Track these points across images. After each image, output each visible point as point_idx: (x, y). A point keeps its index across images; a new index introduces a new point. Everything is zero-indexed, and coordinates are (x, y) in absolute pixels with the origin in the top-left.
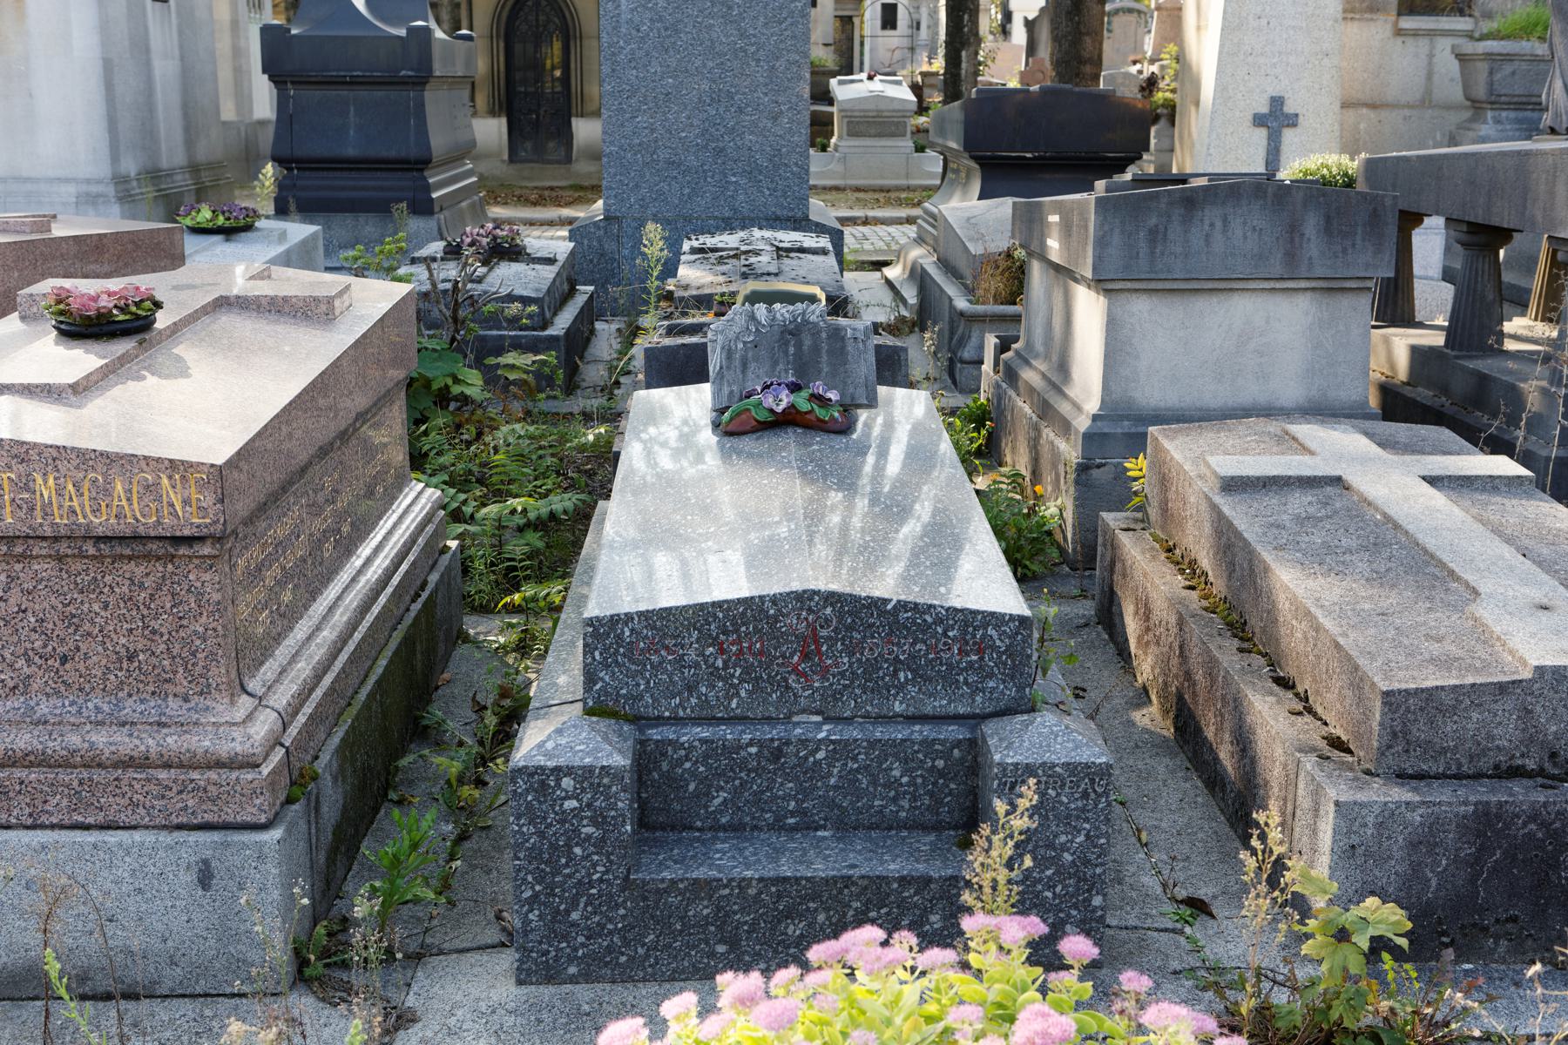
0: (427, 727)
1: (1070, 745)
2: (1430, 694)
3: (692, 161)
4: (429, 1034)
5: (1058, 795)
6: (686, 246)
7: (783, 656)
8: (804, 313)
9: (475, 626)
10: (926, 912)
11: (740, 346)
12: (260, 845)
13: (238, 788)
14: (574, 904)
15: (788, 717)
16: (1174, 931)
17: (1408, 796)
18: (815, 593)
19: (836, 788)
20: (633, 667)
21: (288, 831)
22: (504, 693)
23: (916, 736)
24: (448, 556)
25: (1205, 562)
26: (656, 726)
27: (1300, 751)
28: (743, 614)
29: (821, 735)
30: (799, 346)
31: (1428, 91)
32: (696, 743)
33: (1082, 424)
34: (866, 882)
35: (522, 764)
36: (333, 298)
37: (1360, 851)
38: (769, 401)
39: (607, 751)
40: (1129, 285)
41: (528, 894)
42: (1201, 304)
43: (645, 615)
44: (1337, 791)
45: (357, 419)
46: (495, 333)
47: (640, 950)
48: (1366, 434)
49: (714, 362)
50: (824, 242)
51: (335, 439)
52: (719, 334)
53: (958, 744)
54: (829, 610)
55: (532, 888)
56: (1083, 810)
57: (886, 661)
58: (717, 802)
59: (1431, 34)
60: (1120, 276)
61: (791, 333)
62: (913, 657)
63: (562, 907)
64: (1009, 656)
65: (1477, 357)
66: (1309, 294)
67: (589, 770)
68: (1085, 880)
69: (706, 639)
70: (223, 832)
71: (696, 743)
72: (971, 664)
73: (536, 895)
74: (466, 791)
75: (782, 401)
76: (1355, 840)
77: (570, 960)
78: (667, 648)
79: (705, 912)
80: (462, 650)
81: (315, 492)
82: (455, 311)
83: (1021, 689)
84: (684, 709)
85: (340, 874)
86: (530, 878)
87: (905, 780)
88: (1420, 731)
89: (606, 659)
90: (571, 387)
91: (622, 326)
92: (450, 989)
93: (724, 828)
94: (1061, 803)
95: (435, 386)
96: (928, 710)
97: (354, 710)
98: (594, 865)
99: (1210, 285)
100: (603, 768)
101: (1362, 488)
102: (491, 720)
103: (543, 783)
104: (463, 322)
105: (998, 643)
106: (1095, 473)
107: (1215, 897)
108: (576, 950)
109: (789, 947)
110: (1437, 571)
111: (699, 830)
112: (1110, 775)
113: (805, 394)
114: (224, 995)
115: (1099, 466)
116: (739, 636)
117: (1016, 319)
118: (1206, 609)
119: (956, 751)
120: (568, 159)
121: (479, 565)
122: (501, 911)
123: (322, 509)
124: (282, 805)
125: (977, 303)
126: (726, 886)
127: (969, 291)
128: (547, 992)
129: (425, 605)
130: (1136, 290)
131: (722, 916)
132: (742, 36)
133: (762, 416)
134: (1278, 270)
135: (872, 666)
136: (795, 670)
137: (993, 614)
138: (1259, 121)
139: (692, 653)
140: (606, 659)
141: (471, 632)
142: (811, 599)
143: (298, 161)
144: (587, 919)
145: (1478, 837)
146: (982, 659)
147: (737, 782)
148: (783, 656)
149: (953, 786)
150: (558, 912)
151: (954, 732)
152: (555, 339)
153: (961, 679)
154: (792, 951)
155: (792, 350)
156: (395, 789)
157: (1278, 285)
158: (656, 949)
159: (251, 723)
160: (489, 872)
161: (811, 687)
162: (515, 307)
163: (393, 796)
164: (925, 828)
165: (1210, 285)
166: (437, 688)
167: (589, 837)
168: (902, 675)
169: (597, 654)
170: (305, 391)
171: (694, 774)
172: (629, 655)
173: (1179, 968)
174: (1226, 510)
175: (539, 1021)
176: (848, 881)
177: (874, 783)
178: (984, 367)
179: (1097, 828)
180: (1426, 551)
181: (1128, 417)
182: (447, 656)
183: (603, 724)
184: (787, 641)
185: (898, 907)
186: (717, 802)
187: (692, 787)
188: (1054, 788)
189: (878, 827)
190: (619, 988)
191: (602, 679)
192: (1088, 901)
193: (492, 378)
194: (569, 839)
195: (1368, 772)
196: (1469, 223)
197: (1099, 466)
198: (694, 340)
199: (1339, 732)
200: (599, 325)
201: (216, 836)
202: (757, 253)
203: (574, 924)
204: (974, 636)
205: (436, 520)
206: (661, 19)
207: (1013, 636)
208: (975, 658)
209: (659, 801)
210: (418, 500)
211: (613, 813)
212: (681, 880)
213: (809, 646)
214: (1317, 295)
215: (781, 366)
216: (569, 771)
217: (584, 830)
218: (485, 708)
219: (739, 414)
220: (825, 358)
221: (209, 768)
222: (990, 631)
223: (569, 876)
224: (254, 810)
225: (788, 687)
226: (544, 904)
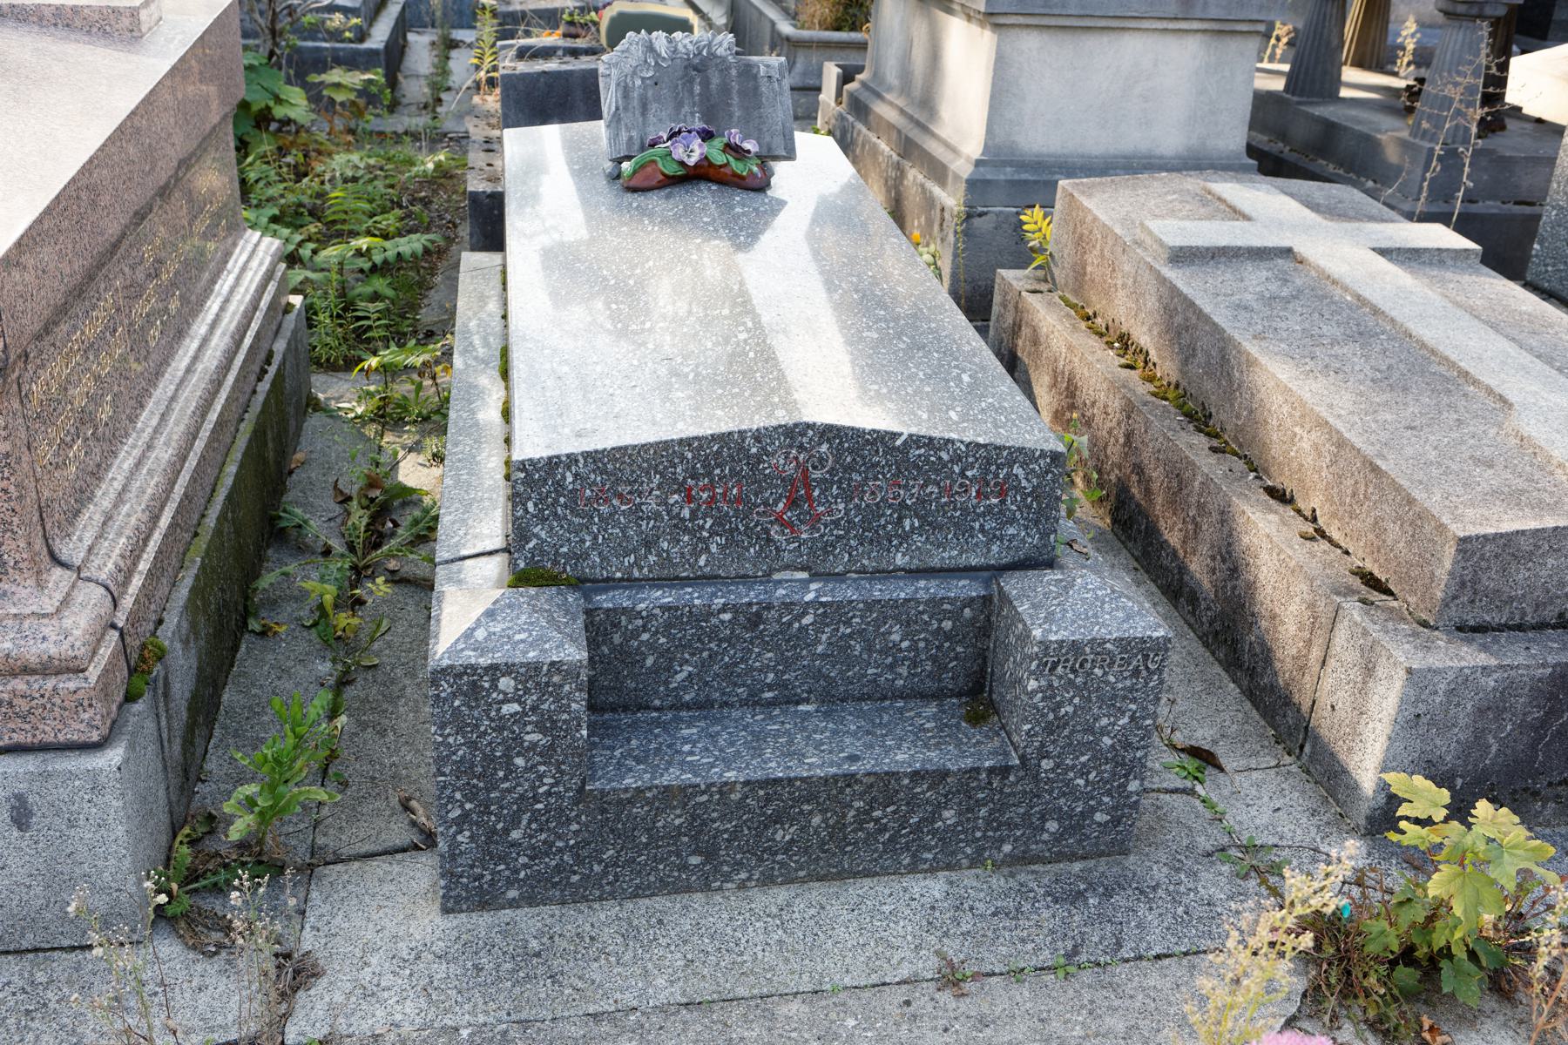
0: (283, 529)
1: (1120, 614)
2: (1507, 541)
4: (339, 998)
5: (1105, 674)
7: (766, 504)
8: (709, 45)
9: (327, 388)
10: (939, 807)
11: (638, 82)
12: (94, 774)
13: (57, 701)
14: (515, 822)
15: (768, 574)
16: (1184, 791)
17: (1483, 659)
18: (809, 426)
19: (823, 656)
20: (577, 520)
21: (131, 747)
22: (372, 483)
23: (921, 595)
24: (292, 317)
25: (1144, 338)
26: (605, 590)
27: (1338, 594)
28: (718, 453)
29: (809, 597)
32: (657, 611)
33: (962, 168)
34: (872, 779)
35: (445, 662)
36: (137, 9)
37: (1424, 720)
38: (679, 153)
39: (551, 638)
40: (1021, 20)
41: (457, 812)
42: (1092, 42)
43: (592, 457)
44: (1401, 656)
45: (179, 167)
46: (310, 44)
47: (596, 868)
48: (1292, 195)
49: (609, 99)
51: (153, 198)
52: (614, 68)
53: (970, 602)
56: (1132, 689)
57: (890, 506)
58: (679, 677)
60: (1013, 9)
62: (922, 501)
63: (500, 826)
65: (1317, 104)
66: (1199, 36)
67: (535, 667)
68: (1124, 764)
69: (671, 484)
70: (41, 756)
71: (657, 611)
72: (989, 509)
73: (465, 815)
74: (343, 620)
75: (694, 152)
76: (1422, 708)
77: (510, 883)
78: (620, 496)
79: (677, 822)
80: (314, 420)
81: (133, 268)
82: (273, 21)
83: (1045, 535)
84: (641, 568)
85: (199, 751)
86: (458, 796)
87: (905, 644)
88: (1489, 581)
89: (541, 511)
90: (393, 107)
91: (435, 38)
92: (358, 919)
93: (688, 706)
94: (1107, 683)
95: (255, 108)
96: (935, 562)
97: (202, 544)
98: (541, 777)
99: (1103, 23)
100: (553, 664)
101: (1322, 263)
102: (359, 518)
104: (281, 34)
105: (1024, 483)
106: (976, 221)
107: (1215, 742)
108: (517, 872)
109: (776, 853)
110: (1442, 369)
111: (657, 709)
113: (718, 143)
114: (62, 949)
115: (981, 215)
116: (712, 481)
117: (862, 46)
118: (1154, 395)
119: (967, 611)
121: (323, 318)
122: (409, 799)
123: (143, 288)
124: (120, 707)
125: (802, 27)
126: (704, 792)
127: (793, 16)
128: (483, 921)
129: (274, 383)
130: (1028, 26)
131: (698, 825)
133: (671, 169)
135: (874, 512)
136: (779, 520)
137: (1021, 450)
139: (652, 501)
140: (541, 511)
141: (321, 396)
142: (803, 434)
144: (531, 837)
145: (1549, 700)
146: (1003, 502)
147: (705, 654)
148: (766, 504)
149: (959, 649)
150: (494, 831)
151: (965, 588)
152: (373, 53)
153: (977, 525)
155: (697, 89)
156: (256, 616)
157: (1171, 25)
158: (616, 865)
159: (66, 618)
160: (382, 733)
161: (797, 539)
162: (337, 20)
163: (254, 625)
164: (924, 696)
165: (1103, 23)
166: (291, 472)
167: (534, 745)
168: (907, 523)
169: (530, 505)
170: (110, 140)
171: (652, 646)
172: (572, 506)
173: (1209, 848)
174: (1180, 285)
175: (478, 969)
176: (850, 779)
177: (869, 649)
178: (822, 97)
180: (1423, 345)
181: (1010, 163)
182: (299, 428)
183: (546, 596)
184: (771, 486)
185: (908, 804)
186: (679, 677)
187: (650, 661)
188: (1102, 667)
189: (870, 698)
190: (570, 911)
191: (537, 536)
193: (316, 96)
194: (509, 748)
195: (1425, 624)
197: (981, 215)
199: (1369, 566)
200: (411, 37)
201: (30, 763)
203: (513, 844)
204: (996, 476)
207: (1042, 476)
208: (995, 501)
209: (619, 689)
210: (255, 254)
211: (565, 716)
212: (650, 789)
213: (798, 492)
215: (686, 109)
216: (509, 669)
217: (527, 738)
218: (349, 498)
219: (643, 167)
220: (736, 100)
221: (14, 675)
222: (1017, 470)
223: (509, 791)
224: (82, 727)
225: (769, 540)
226: (477, 823)
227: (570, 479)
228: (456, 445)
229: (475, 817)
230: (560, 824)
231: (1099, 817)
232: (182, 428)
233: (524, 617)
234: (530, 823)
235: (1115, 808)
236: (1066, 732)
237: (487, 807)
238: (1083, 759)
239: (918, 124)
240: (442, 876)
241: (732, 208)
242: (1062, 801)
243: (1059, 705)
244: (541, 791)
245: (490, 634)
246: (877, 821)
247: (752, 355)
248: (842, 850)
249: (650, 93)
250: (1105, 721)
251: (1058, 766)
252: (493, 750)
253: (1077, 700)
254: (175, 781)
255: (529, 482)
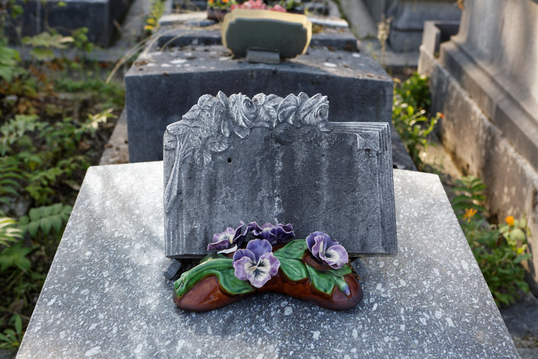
8: (297, 110)
11: (208, 159)
30: (290, 159)
38: (244, 269)
61: (278, 140)
113: (297, 248)
155: (279, 166)
215: (264, 193)
220: (325, 181)
239: (508, 96)
249: (221, 173)
254: (165, 179)
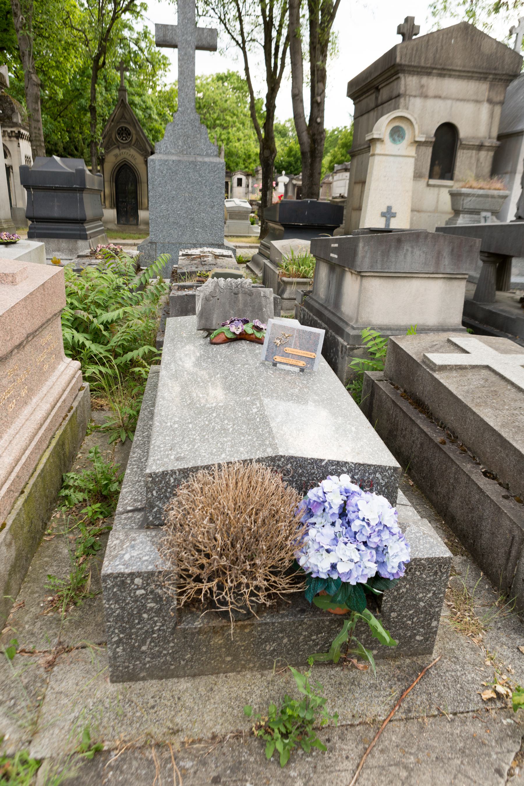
3: (182, 222)
5: (421, 574)
6: (181, 253)
14: (143, 642)
31: (437, 207)
35: (109, 571)
38: (233, 329)
41: (116, 639)
47: (182, 662)
50: (230, 253)
54: (289, 466)
55: (118, 636)
56: (434, 581)
59: (439, 186)
64: (387, 488)
66: (442, 280)
67: (151, 574)
68: (430, 614)
75: (237, 329)
77: (142, 670)
86: (117, 631)
94: (422, 578)
98: (155, 623)
103: (123, 582)
105: (381, 481)
106: (355, 351)
108: (145, 664)
109: (266, 656)
112: (450, 563)
113: (250, 325)
120: (137, 224)
132: (200, 176)
134: (432, 270)
137: (380, 466)
138: (383, 215)
143: (36, 218)
144: (151, 649)
150: (134, 646)
154: (268, 657)
157: (431, 276)
158: (191, 661)
167: (152, 608)
169: (154, 493)
179: (439, 589)
191: (158, 506)
192: (430, 624)
196: (489, 253)
198: (190, 292)
202: (208, 256)
203: (143, 652)
205: (77, 376)
206: (170, 169)
214: (445, 280)
216: (139, 574)
217: (149, 605)
222: (378, 475)
227: (172, 481)
228: (134, 453)
229: (125, 640)
230: (165, 643)
231: (418, 638)
232: (19, 446)
233: (148, 548)
234: (151, 642)
235: (426, 634)
236: (403, 600)
237: (130, 636)
238: (411, 612)
240: (110, 666)
241: (255, 350)
242: (401, 631)
243: (400, 588)
244: (156, 628)
245: (132, 557)
246: (314, 641)
247: (258, 420)
248: (298, 653)
250: (421, 595)
251: (399, 615)
252: (133, 611)
253: (408, 586)
255: (153, 482)
